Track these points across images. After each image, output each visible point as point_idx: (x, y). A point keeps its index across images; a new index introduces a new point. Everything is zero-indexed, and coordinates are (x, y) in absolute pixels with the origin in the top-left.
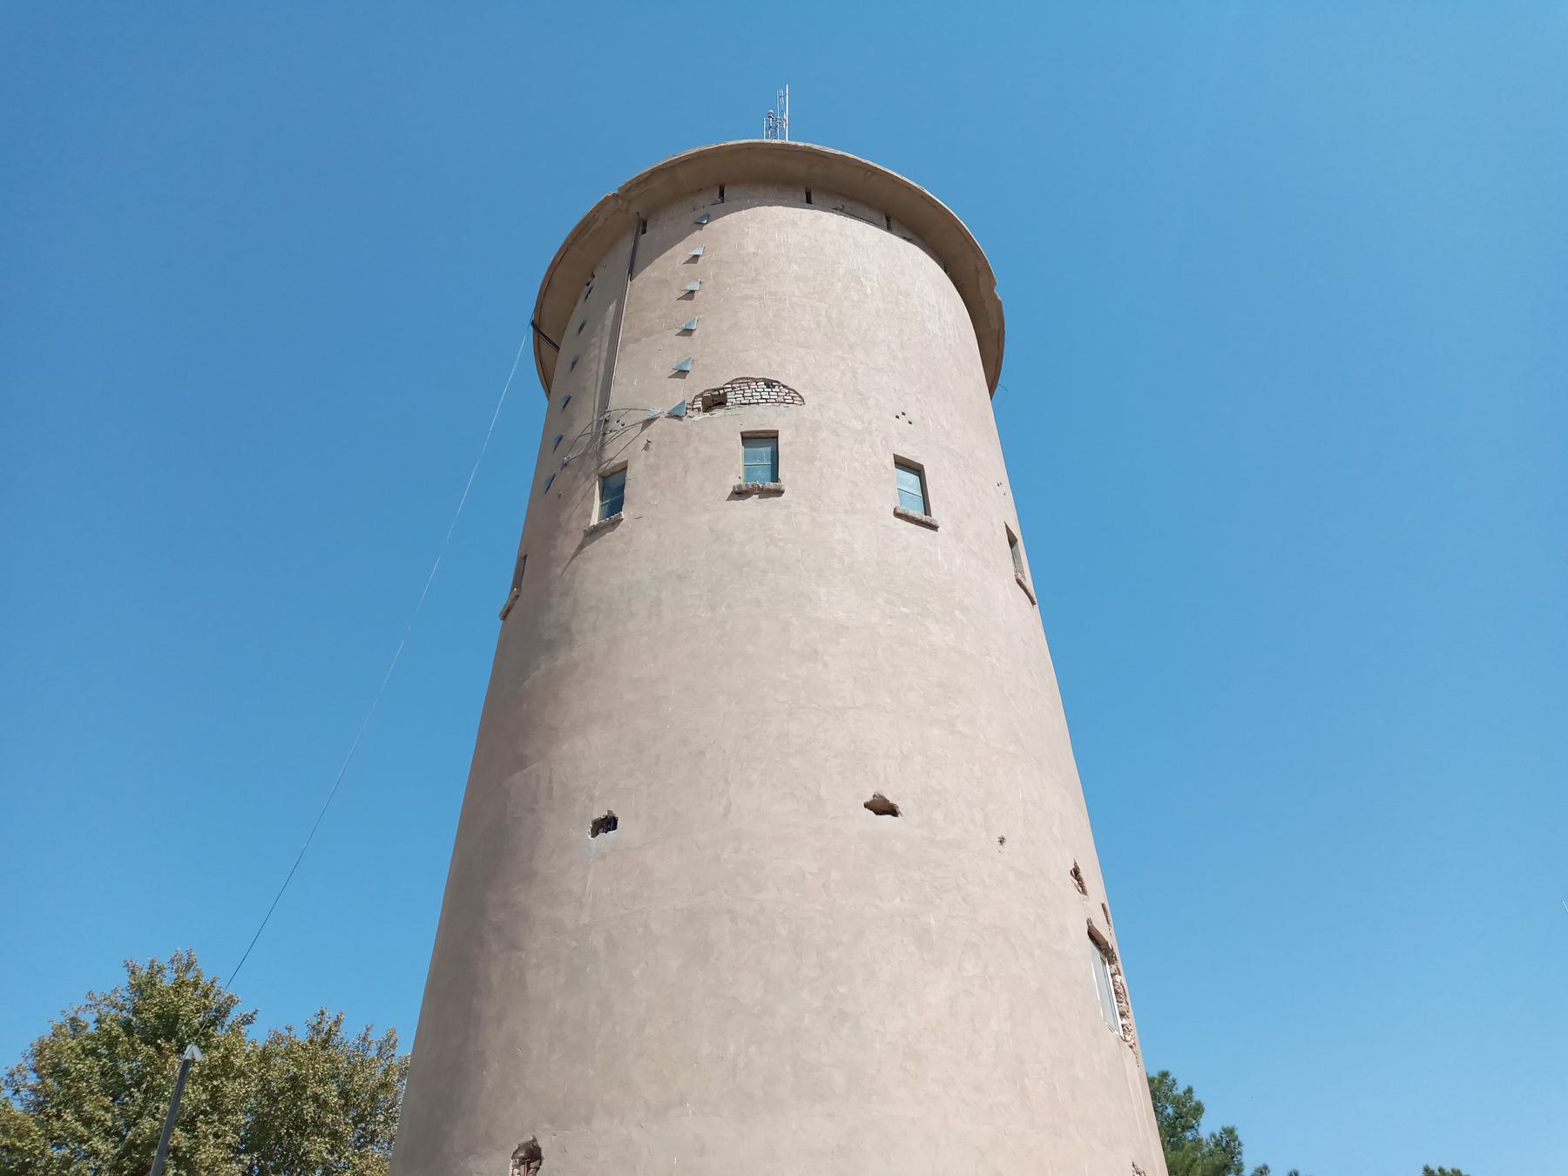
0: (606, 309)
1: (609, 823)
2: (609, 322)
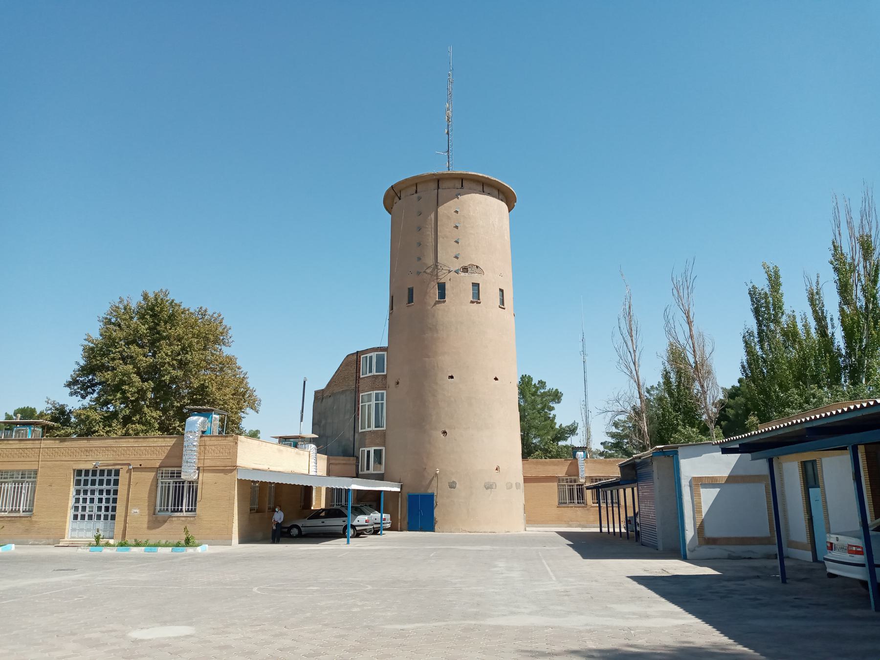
1: (452, 377)
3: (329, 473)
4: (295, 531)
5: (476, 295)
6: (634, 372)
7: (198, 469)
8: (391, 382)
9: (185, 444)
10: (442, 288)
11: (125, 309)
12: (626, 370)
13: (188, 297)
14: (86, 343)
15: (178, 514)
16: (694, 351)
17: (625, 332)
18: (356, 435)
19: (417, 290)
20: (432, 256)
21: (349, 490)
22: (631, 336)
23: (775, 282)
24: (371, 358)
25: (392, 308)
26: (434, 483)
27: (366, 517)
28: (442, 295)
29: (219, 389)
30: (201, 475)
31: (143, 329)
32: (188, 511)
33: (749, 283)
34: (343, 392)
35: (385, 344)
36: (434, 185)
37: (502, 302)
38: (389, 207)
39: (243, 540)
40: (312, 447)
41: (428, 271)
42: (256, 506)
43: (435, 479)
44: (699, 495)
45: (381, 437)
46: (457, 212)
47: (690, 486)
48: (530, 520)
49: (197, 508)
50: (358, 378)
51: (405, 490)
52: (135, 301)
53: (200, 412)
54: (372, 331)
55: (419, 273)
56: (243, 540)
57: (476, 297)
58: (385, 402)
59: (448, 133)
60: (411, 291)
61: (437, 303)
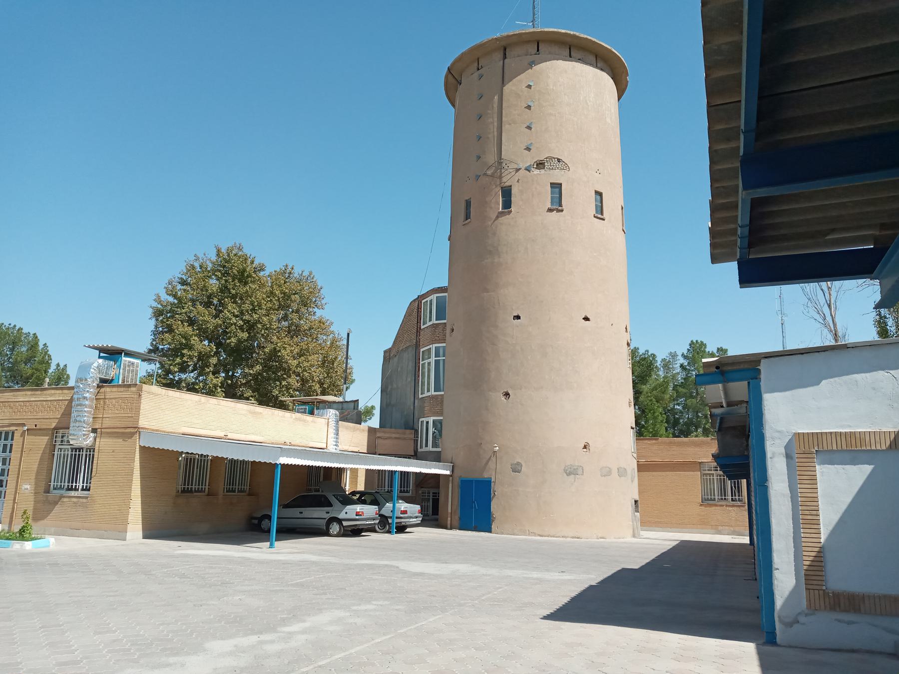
0: (32, 554)
1: (518, 317)
2: (496, 106)
3: (372, 449)
6: (829, 318)
10: (507, 193)
11: (201, 267)
12: (817, 317)
13: (270, 257)
14: (155, 304)
15: (73, 493)
18: (416, 401)
20: (495, 149)
24: (431, 301)
26: (492, 465)
28: (507, 204)
30: (98, 440)
32: (83, 490)
35: (444, 283)
36: (499, 55)
37: (600, 209)
39: (153, 531)
41: (489, 172)
43: (494, 459)
44: (813, 479)
45: (437, 403)
46: (529, 87)
47: (788, 456)
50: (419, 330)
51: (458, 473)
55: (478, 177)
56: (153, 531)
57: (557, 205)
61: (501, 214)
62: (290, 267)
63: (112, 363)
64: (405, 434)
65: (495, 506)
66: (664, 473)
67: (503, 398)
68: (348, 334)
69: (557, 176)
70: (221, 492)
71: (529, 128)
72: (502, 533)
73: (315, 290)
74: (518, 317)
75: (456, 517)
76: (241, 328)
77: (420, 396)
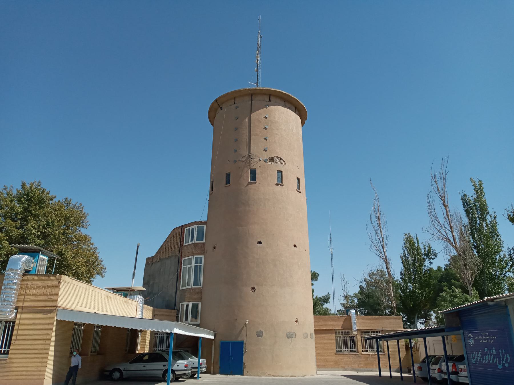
1: (260, 243)
4: (117, 375)
5: (280, 179)
7: (17, 308)
8: (209, 247)
9: (5, 282)
10: (253, 173)
11: (8, 194)
12: (376, 252)
13: (59, 190)
16: (451, 228)
17: (436, 191)
18: (178, 292)
19: (233, 177)
20: (246, 148)
21: (171, 334)
22: (380, 228)
23: (479, 191)
24: (193, 229)
25: (212, 189)
27: (185, 362)
28: (254, 178)
29: (74, 258)
31: (18, 208)
33: (461, 192)
34: (169, 258)
35: (205, 219)
36: (248, 98)
38: (212, 120)
40: (140, 298)
41: (243, 160)
42: (97, 349)
43: (245, 328)
45: (198, 294)
46: (266, 118)
48: (320, 366)
49: (10, 350)
50: (181, 246)
52: (16, 188)
53: (23, 251)
54: (195, 209)
55: (235, 162)
57: (280, 183)
58: (202, 265)
59: (257, 71)
60: (228, 176)
62: (69, 199)
63: (32, 258)
64: (171, 312)
65: (246, 358)
66: (328, 335)
67: (251, 291)
68: (138, 246)
69: (280, 167)
70: (90, 353)
71: (266, 139)
72: (251, 376)
73: (84, 216)
74: (260, 243)
75: (218, 366)
76: (38, 237)
77: (181, 288)
